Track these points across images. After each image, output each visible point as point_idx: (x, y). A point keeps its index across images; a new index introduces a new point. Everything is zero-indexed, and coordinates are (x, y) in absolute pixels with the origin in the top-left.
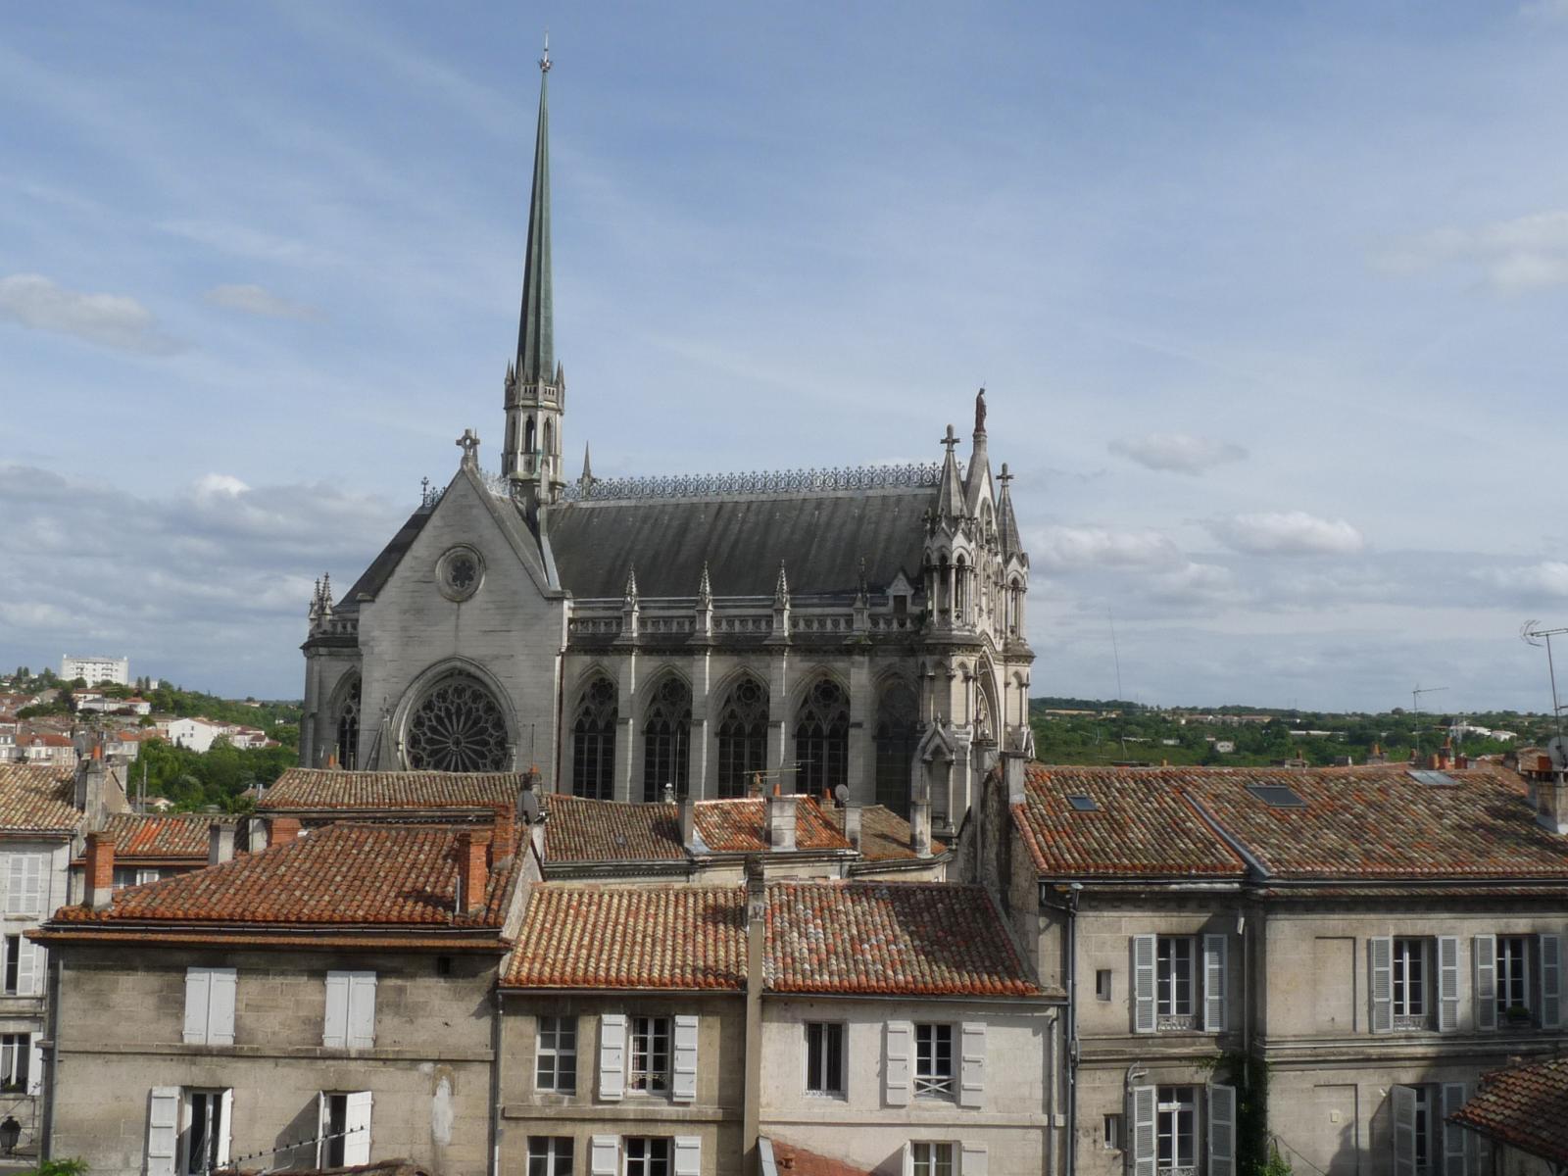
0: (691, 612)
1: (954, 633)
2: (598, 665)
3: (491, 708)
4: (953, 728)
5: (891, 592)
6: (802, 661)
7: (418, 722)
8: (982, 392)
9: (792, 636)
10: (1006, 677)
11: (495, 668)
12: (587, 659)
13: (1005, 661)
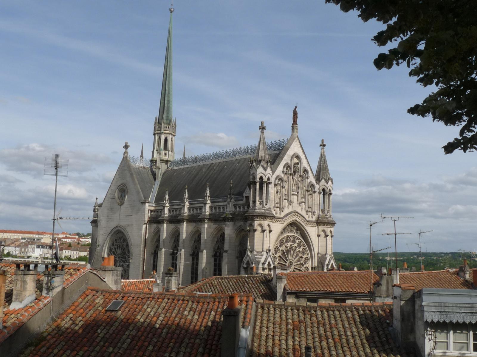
1: (257, 211)
2: (158, 228)
3: (127, 245)
4: (255, 253)
5: (244, 195)
6: (214, 225)
8: (296, 108)
9: (210, 215)
10: (318, 232)
11: (128, 230)
13: (317, 225)
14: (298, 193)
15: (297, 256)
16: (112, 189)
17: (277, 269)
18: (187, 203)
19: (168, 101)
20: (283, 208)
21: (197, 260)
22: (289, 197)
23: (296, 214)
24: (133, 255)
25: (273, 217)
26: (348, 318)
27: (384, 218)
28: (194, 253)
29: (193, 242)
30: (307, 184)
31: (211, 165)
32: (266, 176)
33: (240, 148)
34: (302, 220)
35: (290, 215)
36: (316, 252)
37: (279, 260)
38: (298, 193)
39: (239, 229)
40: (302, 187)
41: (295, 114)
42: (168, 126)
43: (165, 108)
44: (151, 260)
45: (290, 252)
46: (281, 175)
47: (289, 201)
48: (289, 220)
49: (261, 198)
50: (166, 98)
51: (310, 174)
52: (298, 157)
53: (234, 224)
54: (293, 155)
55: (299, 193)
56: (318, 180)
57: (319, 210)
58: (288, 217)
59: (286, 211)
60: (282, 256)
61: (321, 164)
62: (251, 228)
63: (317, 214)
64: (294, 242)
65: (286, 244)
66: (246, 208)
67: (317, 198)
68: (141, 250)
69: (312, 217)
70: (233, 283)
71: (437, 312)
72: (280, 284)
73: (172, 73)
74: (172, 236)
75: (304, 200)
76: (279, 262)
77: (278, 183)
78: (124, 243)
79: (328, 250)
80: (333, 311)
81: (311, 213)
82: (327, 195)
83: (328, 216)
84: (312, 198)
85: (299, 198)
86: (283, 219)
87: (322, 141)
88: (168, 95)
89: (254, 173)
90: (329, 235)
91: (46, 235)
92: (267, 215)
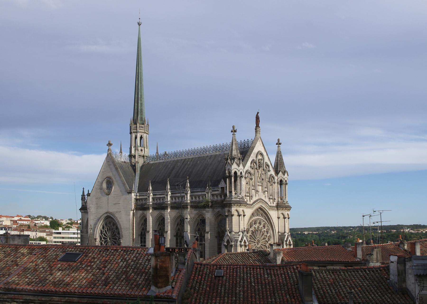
0: (146, 197)
2: (144, 214)
3: (117, 228)
4: (233, 233)
5: (220, 186)
6: (194, 211)
7: (101, 233)
8: (258, 113)
10: (278, 215)
11: (117, 215)
12: (141, 212)
14: (262, 184)
15: (262, 235)
16: (99, 181)
17: (273, 246)
18: (170, 193)
19: (141, 104)
20: (252, 197)
21: (145, 238)
22: (256, 188)
23: (262, 201)
24: (124, 236)
25: (246, 204)
26: (361, 276)
27: (375, 212)
28: (142, 233)
29: (176, 226)
30: (268, 176)
31: (185, 160)
32: (239, 171)
33: (210, 146)
34: (266, 206)
36: (277, 232)
37: (250, 238)
38: (262, 184)
39: (217, 214)
40: (265, 179)
41: (257, 118)
42: (142, 126)
43: (139, 110)
44: (138, 240)
45: (258, 232)
46: (249, 170)
47: (256, 190)
48: (257, 206)
49: (235, 189)
50: (139, 101)
51: (271, 169)
52: (262, 154)
53: (213, 210)
54: (258, 153)
55: (263, 184)
56: (277, 173)
57: (278, 197)
59: (254, 199)
60: (252, 235)
61: (278, 159)
62: (229, 213)
63: (276, 200)
64: (260, 223)
65: (254, 226)
66: (223, 197)
67: (276, 187)
68: (130, 232)
69: (273, 203)
70: (240, 257)
71: (423, 269)
72: (279, 257)
73: (143, 79)
74: (157, 220)
75: (266, 189)
76: (250, 240)
77: (247, 177)
78: (113, 226)
79: (286, 229)
80: (351, 272)
81: (272, 200)
82: (284, 185)
83: (285, 202)
84: (272, 187)
85: (263, 188)
86: (252, 205)
87: (278, 140)
88: (141, 99)
89: (229, 169)
90: (286, 218)
91: (3, 218)
92: (241, 202)
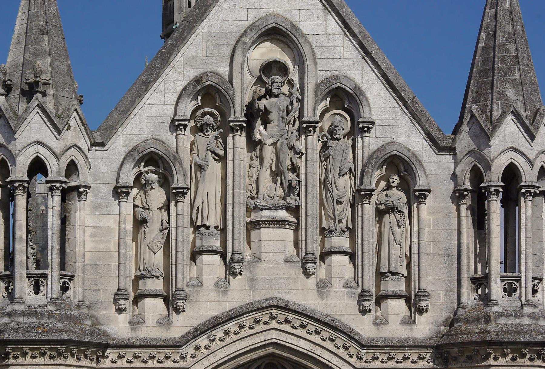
35: (232, 326)
58: (219, 333)
